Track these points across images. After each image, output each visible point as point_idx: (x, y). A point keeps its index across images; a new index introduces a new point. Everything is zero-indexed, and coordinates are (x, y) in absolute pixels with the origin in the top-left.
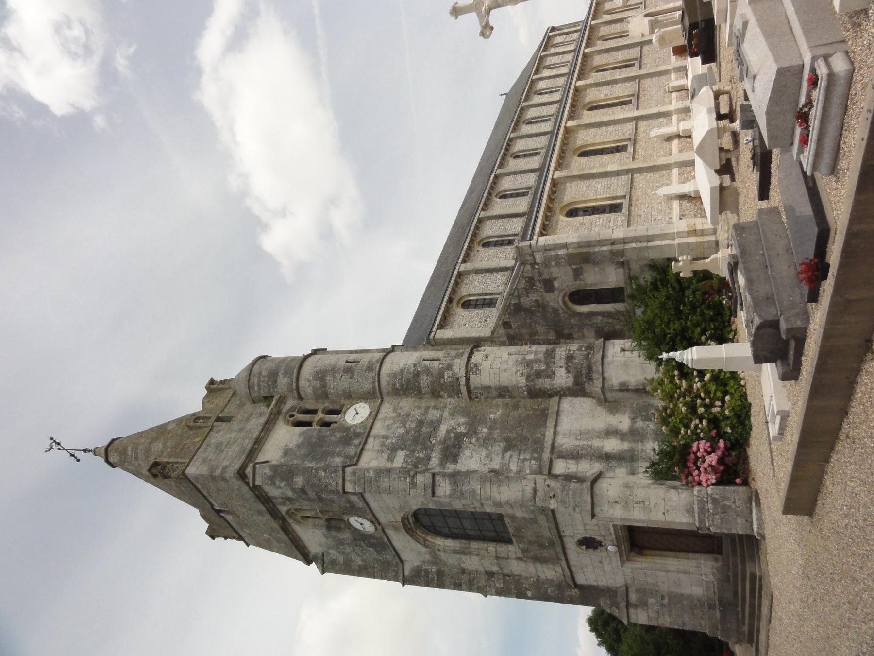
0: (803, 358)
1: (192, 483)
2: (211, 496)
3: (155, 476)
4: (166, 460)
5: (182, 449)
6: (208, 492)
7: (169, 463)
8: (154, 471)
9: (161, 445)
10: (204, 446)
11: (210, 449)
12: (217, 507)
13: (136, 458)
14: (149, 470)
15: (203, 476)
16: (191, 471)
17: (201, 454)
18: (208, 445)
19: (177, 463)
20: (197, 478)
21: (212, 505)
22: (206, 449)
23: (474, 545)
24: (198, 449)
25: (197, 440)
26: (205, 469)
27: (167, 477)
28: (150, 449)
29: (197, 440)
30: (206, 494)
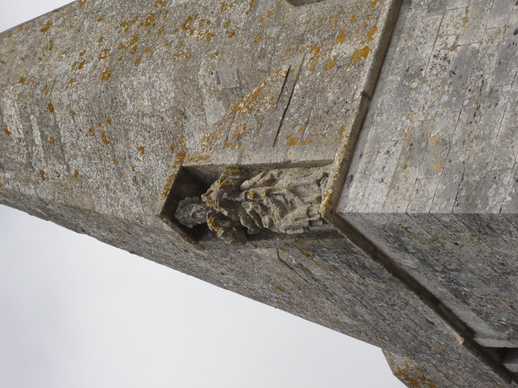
0: (212, 186)
1: (376, 253)
2: (464, 299)
3: (197, 233)
4: (230, 158)
5: (283, 99)
6: (451, 283)
7: (246, 172)
8: (193, 212)
9: (165, 84)
10: (391, 79)
11: (424, 94)
12: (491, 339)
13: (54, 145)
14: (169, 212)
15: (429, 219)
16: (368, 199)
17: (388, 124)
18: (412, 74)
19: (287, 165)
20: (398, 231)
21: (469, 334)
22: (403, 90)
23: (396, 279)
24: (368, 96)
25: (346, 49)
26: (434, 186)
27: (252, 233)
28: (115, 103)
29: (346, 49)
30: (437, 290)
